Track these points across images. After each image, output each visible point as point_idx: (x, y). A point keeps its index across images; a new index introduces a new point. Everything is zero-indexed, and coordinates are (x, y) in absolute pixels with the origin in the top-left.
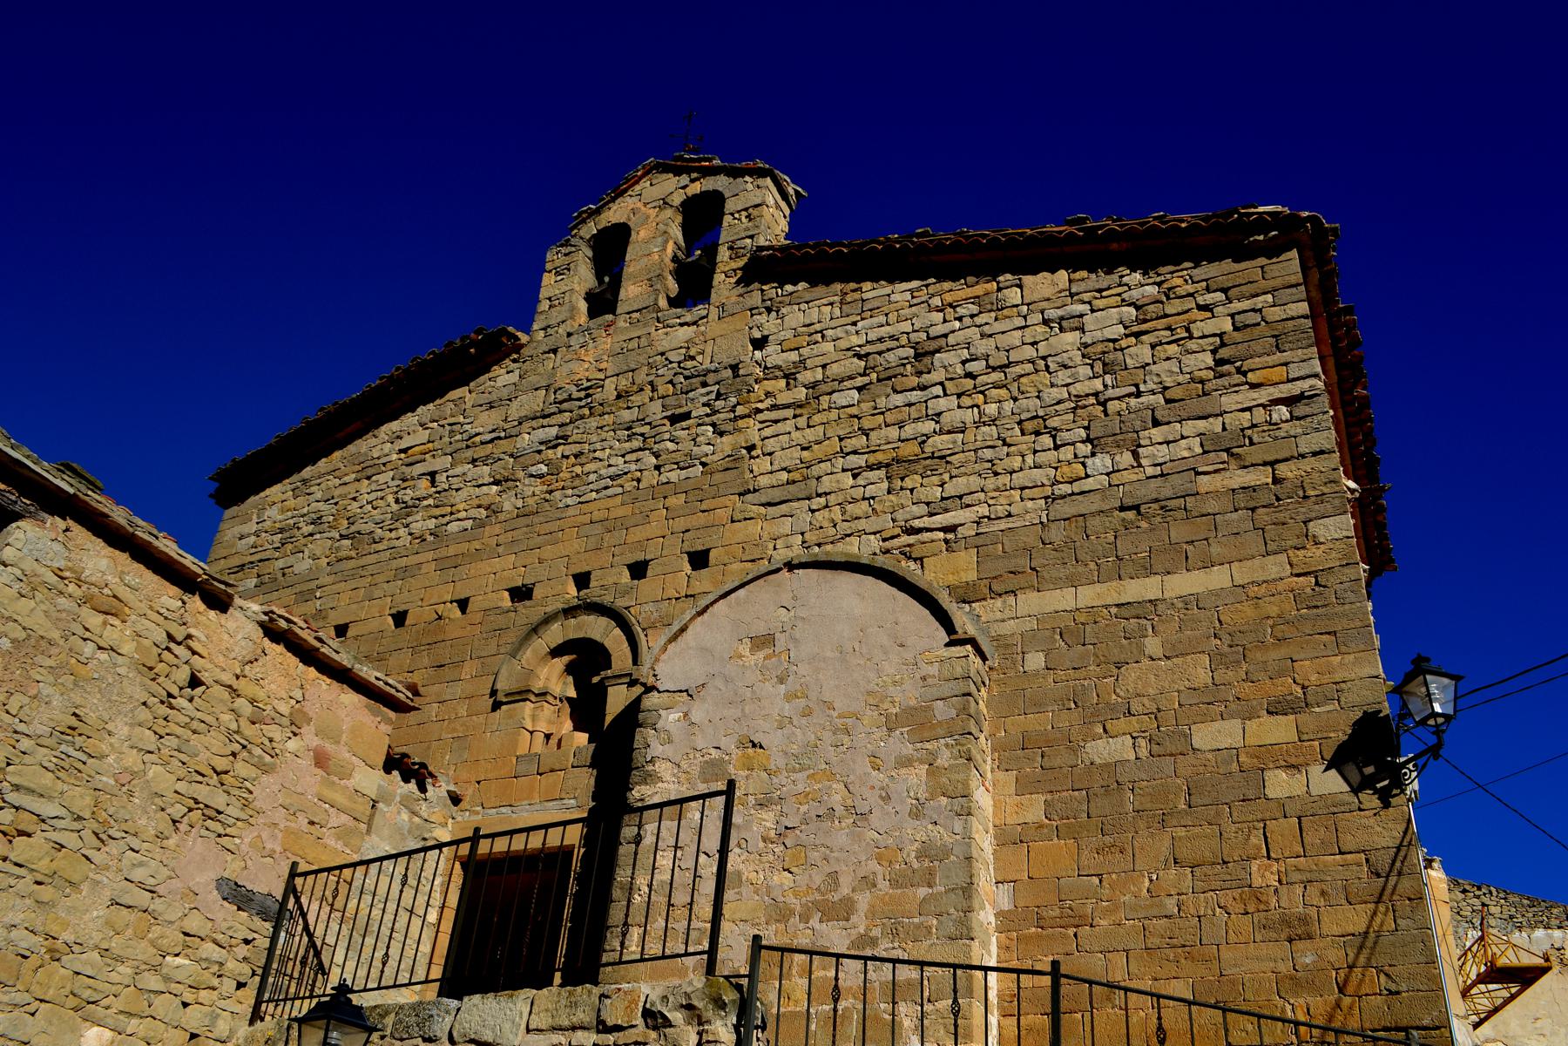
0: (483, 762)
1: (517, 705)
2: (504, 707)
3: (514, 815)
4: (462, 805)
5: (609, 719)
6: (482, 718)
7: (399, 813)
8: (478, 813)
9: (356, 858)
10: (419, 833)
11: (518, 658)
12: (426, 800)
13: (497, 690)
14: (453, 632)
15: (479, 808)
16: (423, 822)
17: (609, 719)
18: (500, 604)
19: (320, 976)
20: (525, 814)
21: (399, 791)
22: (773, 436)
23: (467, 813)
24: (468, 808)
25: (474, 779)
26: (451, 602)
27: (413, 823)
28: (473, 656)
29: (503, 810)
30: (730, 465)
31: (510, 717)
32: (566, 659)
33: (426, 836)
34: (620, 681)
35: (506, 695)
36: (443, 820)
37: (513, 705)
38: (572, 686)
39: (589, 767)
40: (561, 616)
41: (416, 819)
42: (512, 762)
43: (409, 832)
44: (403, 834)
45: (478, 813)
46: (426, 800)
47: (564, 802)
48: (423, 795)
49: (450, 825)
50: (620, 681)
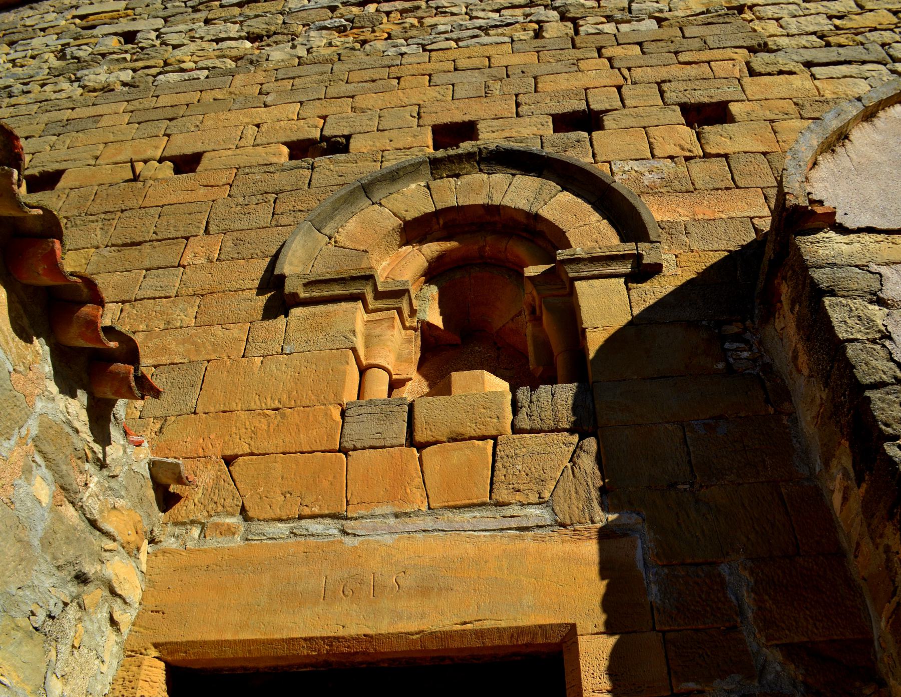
0: (243, 415)
1: (332, 307)
2: (296, 312)
3: (348, 540)
4: (179, 510)
5: (592, 354)
6: (238, 332)
7: (27, 472)
8: (230, 531)
9: (191, 81)
10: (70, 553)
11: (327, 230)
12: (102, 465)
13: (282, 277)
14: (157, 195)
15: (235, 520)
16: (84, 526)
17: (592, 354)
18: (274, 160)
19: (100, 456)
20: (388, 539)
21: (40, 405)
22: (727, 47)
23: (196, 532)
24: (201, 516)
25: (217, 451)
26: (160, 161)
27: (60, 519)
28: (212, 228)
29: (315, 526)
30: (710, 20)
31: (317, 328)
32: (433, 249)
33: (90, 569)
34: (607, 270)
35: (308, 285)
36: (133, 538)
37: (320, 308)
38: (436, 305)
39: (571, 431)
40: (426, 170)
41: (69, 511)
42: (330, 417)
43: (46, 543)
44: (27, 545)
45: (230, 531)
46: (102, 465)
47: (509, 511)
48: (97, 448)
49: (143, 557)
50: (607, 270)
